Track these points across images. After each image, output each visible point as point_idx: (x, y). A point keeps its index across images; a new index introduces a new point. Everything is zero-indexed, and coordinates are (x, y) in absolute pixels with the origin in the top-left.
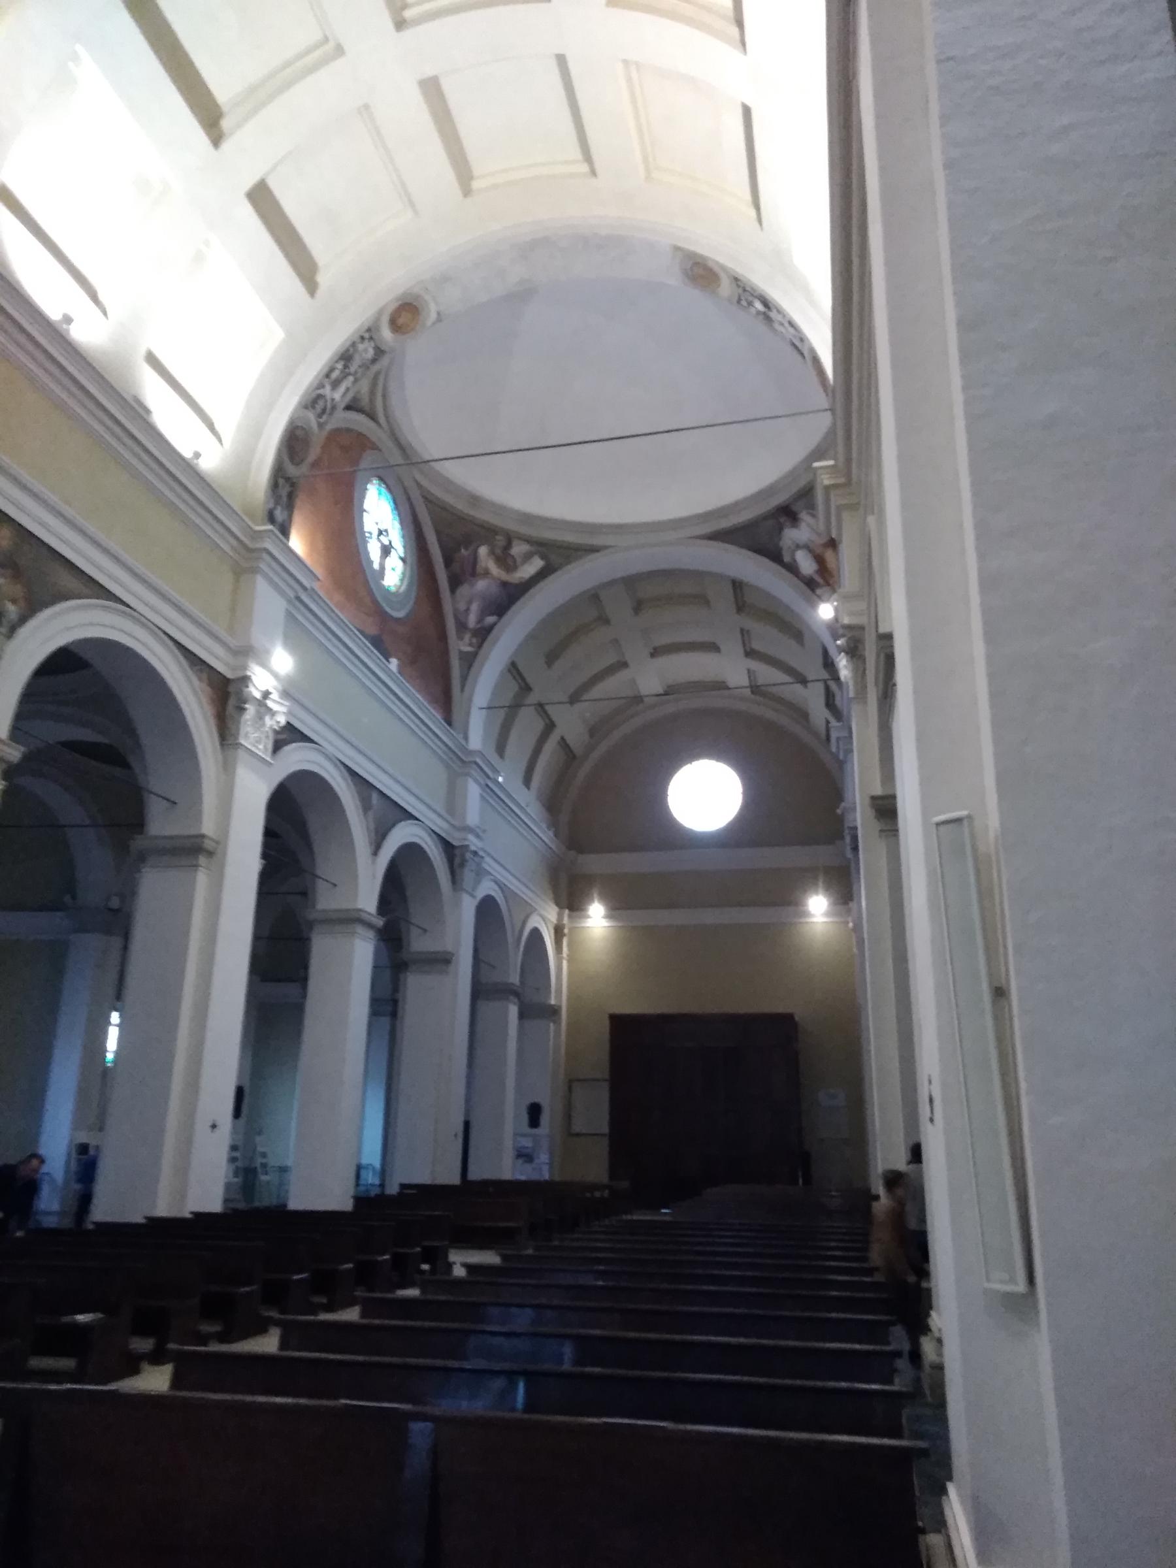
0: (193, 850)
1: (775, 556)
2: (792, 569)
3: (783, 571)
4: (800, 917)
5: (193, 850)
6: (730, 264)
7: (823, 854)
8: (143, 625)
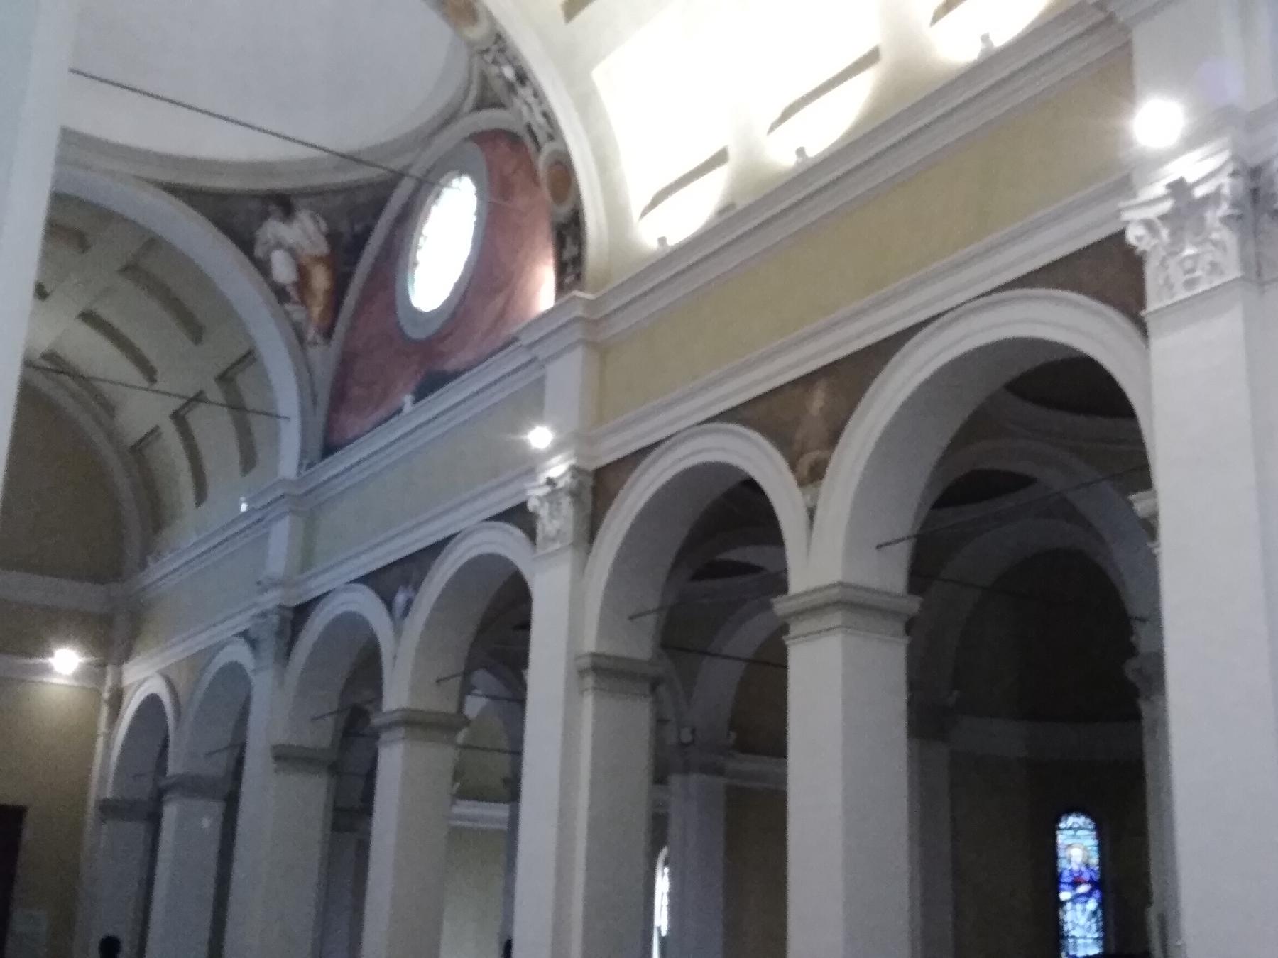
0: (605, 672)
1: (246, 244)
2: (263, 268)
3: (252, 268)
4: (83, 688)
5: (605, 672)
6: (495, 12)
7: (88, 596)
8: (692, 436)
